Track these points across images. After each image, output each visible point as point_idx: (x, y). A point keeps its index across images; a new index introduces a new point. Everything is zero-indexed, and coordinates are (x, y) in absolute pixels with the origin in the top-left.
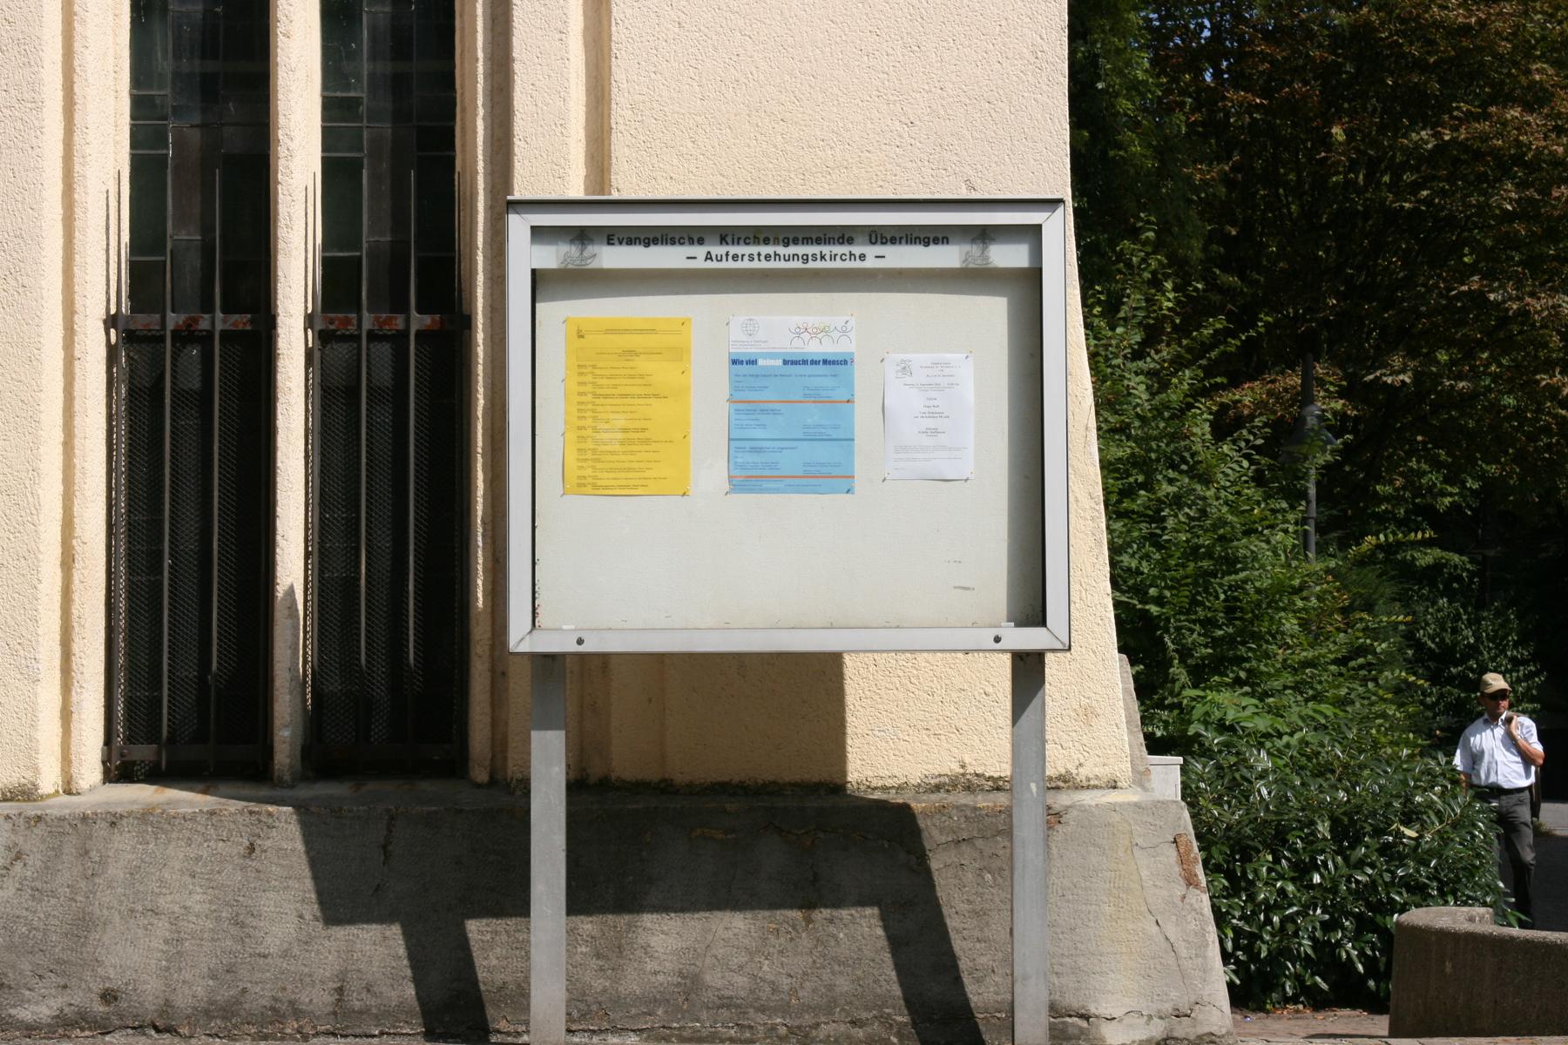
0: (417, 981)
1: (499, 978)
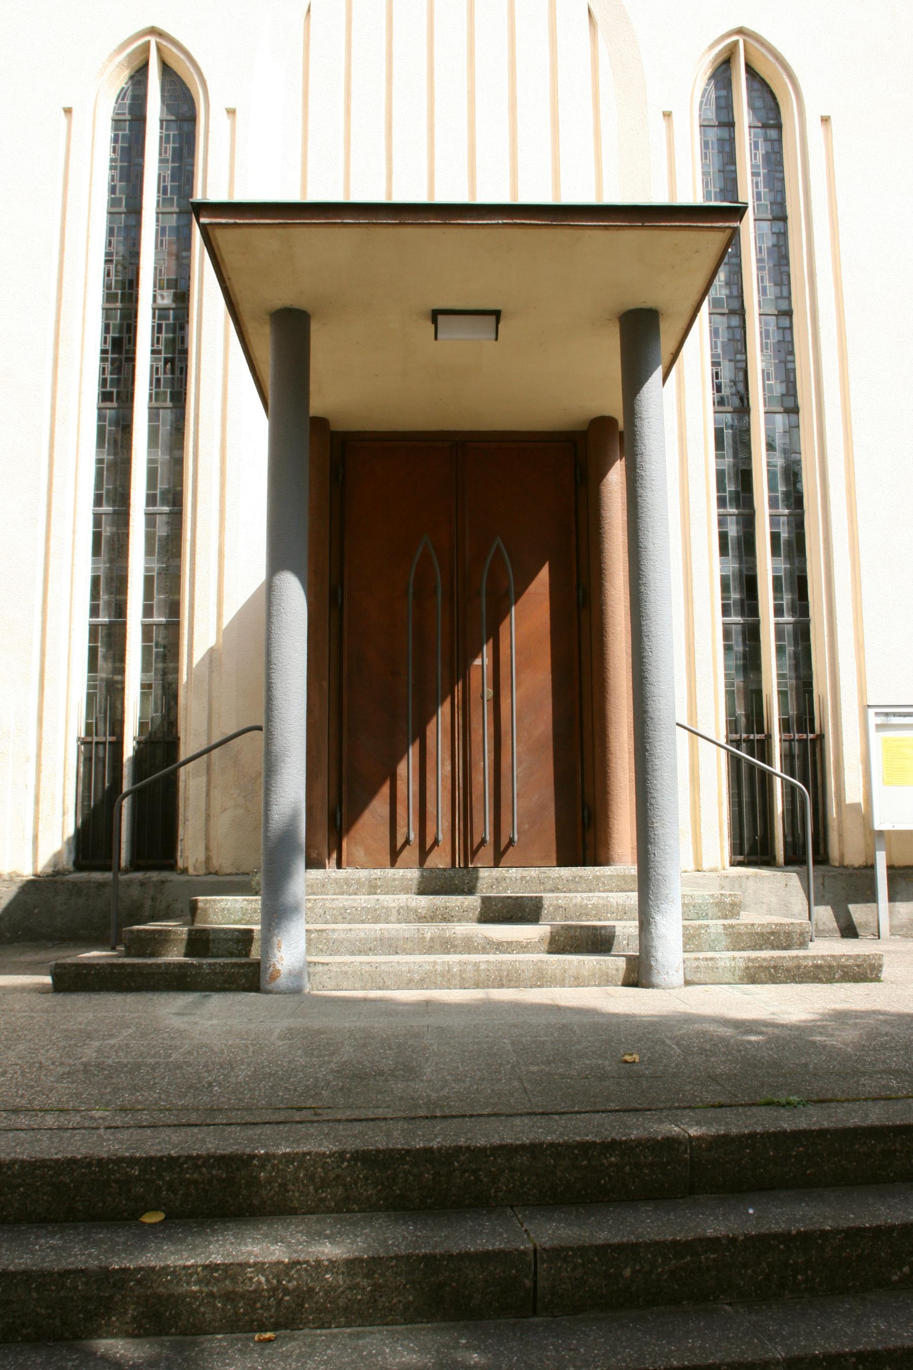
0: (837, 921)
1: (860, 921)
